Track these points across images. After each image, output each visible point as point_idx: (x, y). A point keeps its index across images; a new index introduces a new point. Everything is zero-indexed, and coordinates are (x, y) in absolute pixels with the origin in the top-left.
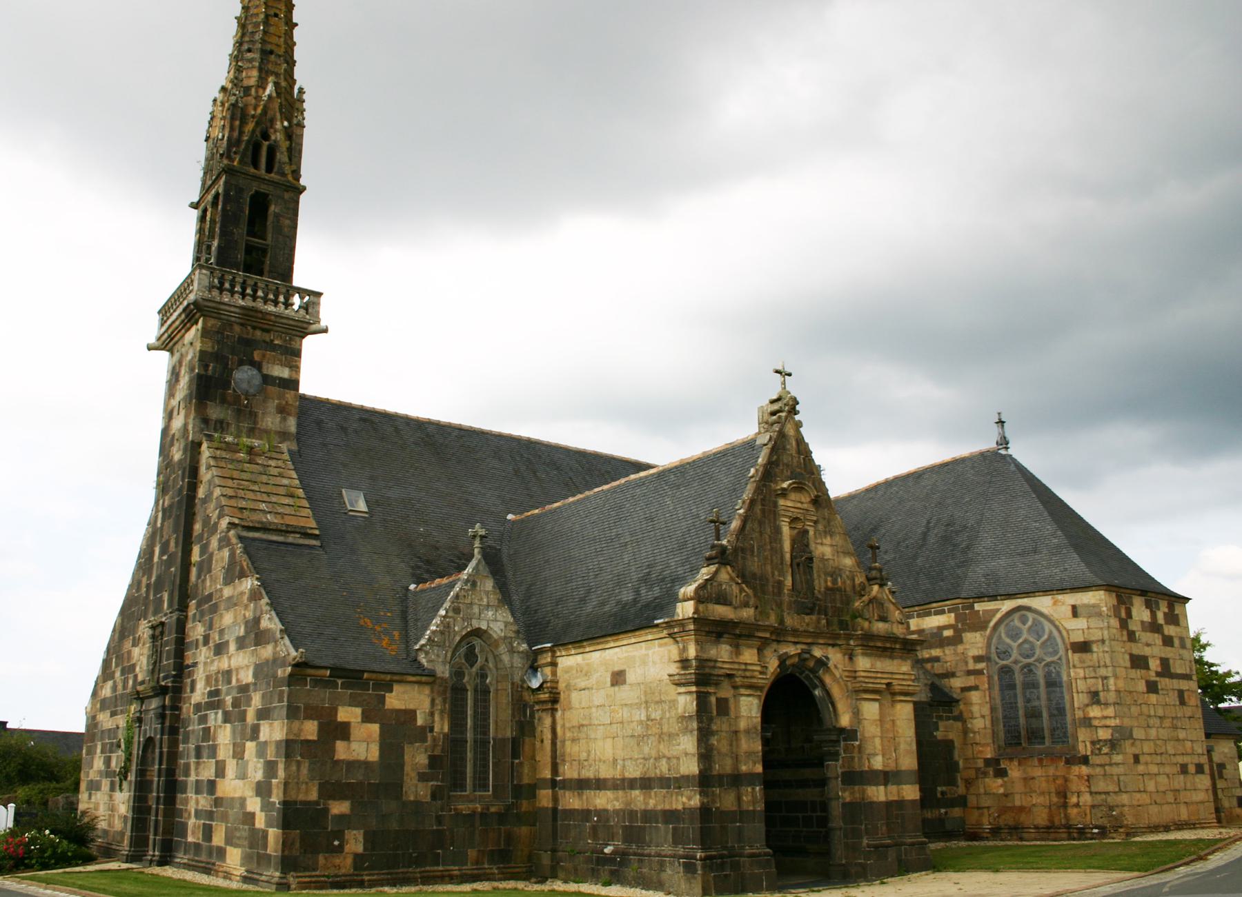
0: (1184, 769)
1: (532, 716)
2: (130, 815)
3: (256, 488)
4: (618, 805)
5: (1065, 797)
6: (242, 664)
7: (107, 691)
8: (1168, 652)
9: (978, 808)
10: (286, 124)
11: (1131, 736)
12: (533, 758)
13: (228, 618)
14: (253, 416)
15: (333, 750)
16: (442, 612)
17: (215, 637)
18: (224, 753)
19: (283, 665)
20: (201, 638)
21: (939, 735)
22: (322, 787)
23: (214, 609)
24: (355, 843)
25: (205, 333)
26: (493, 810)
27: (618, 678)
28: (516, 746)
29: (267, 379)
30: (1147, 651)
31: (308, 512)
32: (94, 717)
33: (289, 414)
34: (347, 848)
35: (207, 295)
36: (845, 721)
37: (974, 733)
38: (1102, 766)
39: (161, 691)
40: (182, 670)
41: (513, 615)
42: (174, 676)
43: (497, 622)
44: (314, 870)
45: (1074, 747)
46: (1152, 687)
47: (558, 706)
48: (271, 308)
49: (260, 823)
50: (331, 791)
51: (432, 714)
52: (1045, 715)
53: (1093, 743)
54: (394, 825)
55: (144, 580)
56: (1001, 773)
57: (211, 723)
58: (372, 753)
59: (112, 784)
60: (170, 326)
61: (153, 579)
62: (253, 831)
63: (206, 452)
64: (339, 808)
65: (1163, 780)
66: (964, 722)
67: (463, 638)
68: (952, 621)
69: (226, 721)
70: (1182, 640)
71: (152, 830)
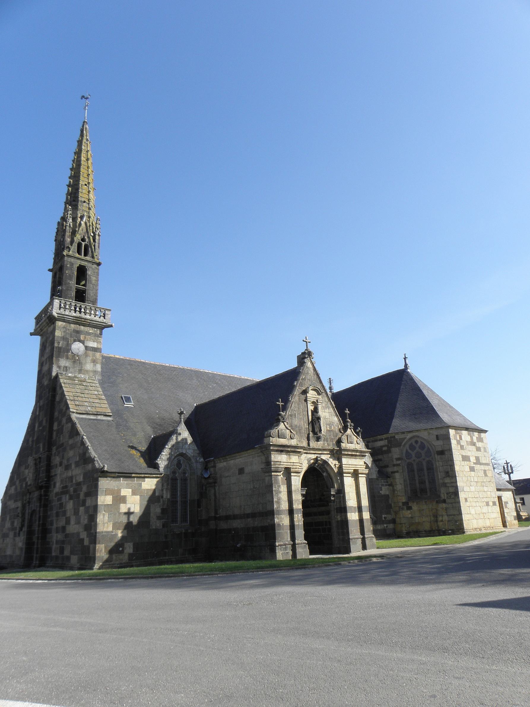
0: (487, 504)
1: (206, 490)
2: (24, 547)
5: (437, 517)
8: (478, 454)
9: (401, 524)
14: (80, 363)
15: (119, 508)
17: (65, 462)
20: (58, 463)
21: (382, 492)
26: (189, 531)
29: (86, 347)
30: (469, 454)
31: (107, 406)
33: (97, 363)
34: (125, 551)
37: (397, 491)
38: (451, 503)
39: (41, 488)
40: (49, 478)
41: (197, 446)
42: (46, 481)
44: (111, 561)
45: (439, 496)
46: (472, 469)
47: (216, 484)
48: (88, 317)
53: (447, 494)
55: (31, 439)
56: (409, 508)
57: (63, 500)
60: (333, 569)
61: (35, 438)
66: (393, 487)
67: (175, 457)
68: (386, 443)
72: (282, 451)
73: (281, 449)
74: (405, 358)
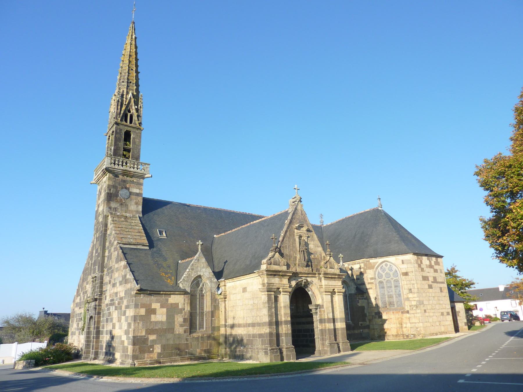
2: (85, 343)
3: (127, 230)
4: (245, 333)
6: (121, 290)
7: (78, 300)
10: (136, 107)
11: (423, 304)
12: (219, 317)
13: (116, 275)
14: (127, 206)
16: (188, 270)
17: (113, 281)
18: (115, 320)
19: (134, 290)
21: (359, 305)
22: (146, 330)
23: (112, 272)
24: (158, 349)
25: (109, 179)
27: (244, 290)
28: (213, 314)
29: (131, 193)
30: (428, 275)
32: (74, 309)
35: (110, 166)
36: (319, 302)
39: (96, 300)
40: (102, 293)
43: (206, 273)
44: (144, 359)
45: (404, 308)
46: (430, 287)
47: (226, 299)
48: (132, 169)
49: (126, 344)
50: (150, 332)
51: (184, 304)
52: (394, 296)
53: (410, 306)
54: (171, 342)
57: (111, 310)
58: (164, 318)
59: (79, 332)
62: (124, 347)
63: (110, 219)
64: (152, 337)
65: (435, 318)
69: (116, 309)
70: (441, 270)
71: (91, 348)
72: (275, 275)
73: (274, 273)
74: (225, 263)
